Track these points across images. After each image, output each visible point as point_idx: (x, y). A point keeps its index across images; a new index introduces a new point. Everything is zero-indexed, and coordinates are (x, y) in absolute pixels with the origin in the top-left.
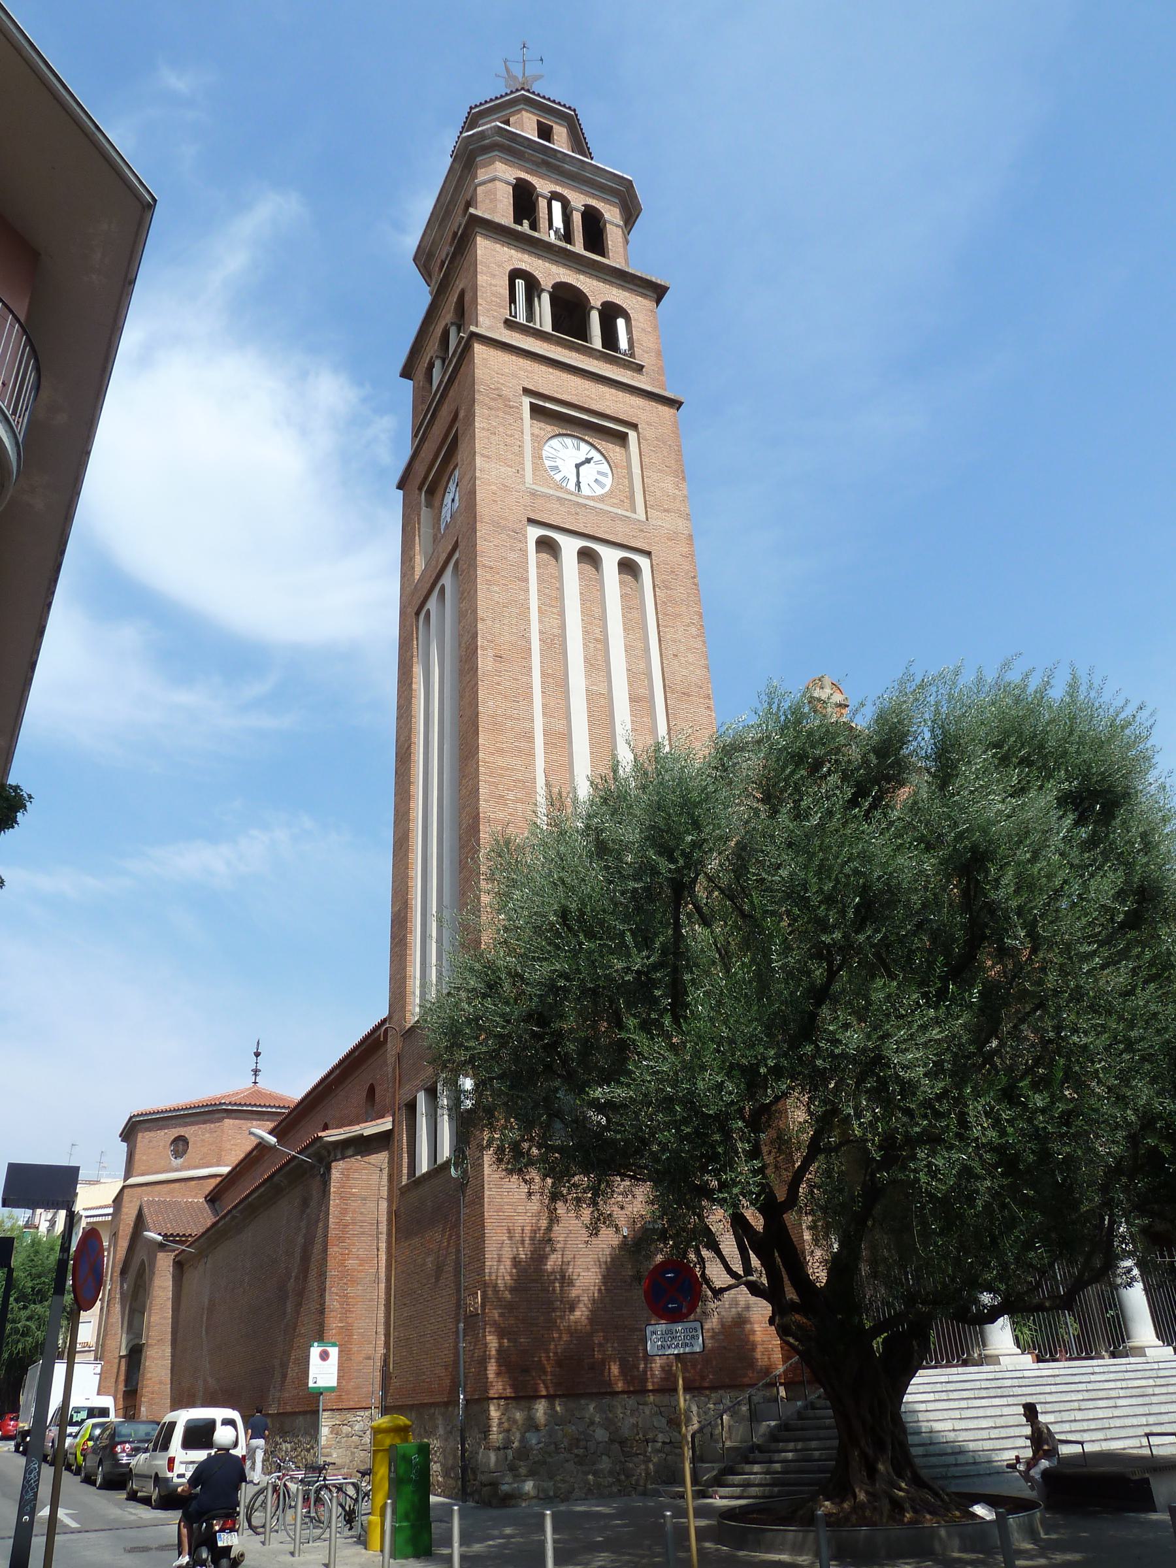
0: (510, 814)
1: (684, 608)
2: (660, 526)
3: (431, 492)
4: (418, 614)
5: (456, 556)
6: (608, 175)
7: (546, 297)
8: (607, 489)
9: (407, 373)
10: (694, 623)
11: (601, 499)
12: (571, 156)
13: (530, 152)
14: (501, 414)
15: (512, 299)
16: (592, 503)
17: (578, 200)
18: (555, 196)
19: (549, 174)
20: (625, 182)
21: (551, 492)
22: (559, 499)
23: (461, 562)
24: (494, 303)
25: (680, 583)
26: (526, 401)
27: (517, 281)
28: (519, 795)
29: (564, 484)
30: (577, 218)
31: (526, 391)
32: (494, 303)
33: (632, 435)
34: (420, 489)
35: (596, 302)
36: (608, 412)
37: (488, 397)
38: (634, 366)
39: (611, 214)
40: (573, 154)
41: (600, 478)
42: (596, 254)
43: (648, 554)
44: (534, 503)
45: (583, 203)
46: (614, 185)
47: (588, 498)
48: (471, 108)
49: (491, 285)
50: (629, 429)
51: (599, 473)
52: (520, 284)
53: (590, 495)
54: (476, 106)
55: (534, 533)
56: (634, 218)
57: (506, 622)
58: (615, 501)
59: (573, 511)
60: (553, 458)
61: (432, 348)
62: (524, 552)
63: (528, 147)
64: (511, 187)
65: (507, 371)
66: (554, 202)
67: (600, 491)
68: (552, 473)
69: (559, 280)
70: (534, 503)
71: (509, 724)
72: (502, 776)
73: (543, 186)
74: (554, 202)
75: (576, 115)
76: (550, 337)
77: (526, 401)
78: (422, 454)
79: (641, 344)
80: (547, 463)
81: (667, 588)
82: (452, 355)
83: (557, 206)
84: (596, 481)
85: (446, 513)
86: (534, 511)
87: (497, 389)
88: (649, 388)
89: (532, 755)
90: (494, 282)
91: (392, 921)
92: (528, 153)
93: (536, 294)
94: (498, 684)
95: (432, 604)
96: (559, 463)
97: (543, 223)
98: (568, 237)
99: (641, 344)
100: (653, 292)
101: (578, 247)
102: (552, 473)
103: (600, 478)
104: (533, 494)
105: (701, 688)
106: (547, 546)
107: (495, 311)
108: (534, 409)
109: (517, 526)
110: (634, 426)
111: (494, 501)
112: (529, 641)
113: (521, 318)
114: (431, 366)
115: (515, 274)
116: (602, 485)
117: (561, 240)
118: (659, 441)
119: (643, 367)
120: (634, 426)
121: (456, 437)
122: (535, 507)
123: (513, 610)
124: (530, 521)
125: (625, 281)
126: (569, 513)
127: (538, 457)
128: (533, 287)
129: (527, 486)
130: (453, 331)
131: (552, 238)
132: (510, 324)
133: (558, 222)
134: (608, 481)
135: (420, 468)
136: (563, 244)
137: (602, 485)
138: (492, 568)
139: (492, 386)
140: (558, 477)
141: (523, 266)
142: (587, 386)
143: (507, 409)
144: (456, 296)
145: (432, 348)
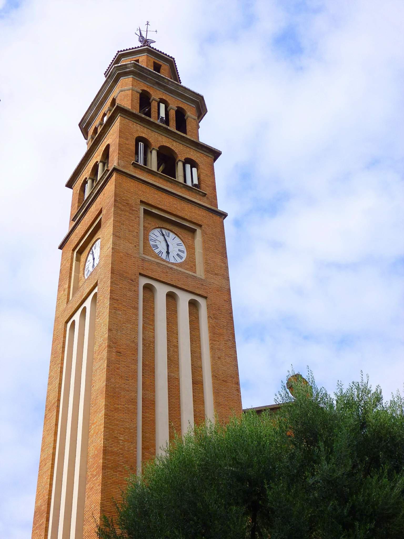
0: (121, 449)
1: (225, 331)
2: (213, 283)
3: (80, 252)
4: (67, 322)
5: (96, 290)
6: (191, 93)
7: (154, 153)
8: (183, 260)
9: (70, 185)
10: (230, 340)
11: (180, 265)
12: (153, 72)
13: (150, 77)
14: (127, 214)
15: (137, 153)
16: (175, 267)
17: (174, 103)
18: (162, 101)
19: (159, 89)
20: (200, 97)
21: (153, 259)
22: (158, 263)
23: (98, 296)
24: (127, 154)
25: (223, 316)
26: (142, 208)
27: (140, 143)
28: (126, 438)
29: (160, 255)
30: (172, 114)
31: (142, 202)
32: (127, 154)
33: (199, 232)
34: (74, 250)
35: (181, 157)
36: (186, 217)
37: (121, 204)
38: (201, 193)
39: (190, 113)
40: (154, 72)
41: (180, 253)
42: (182, 133)
43: (206, 298)
44: (143, 265)
45: (142, 89)
46: (194, 98)
47: (173, 264)
48: (118, 52)
49: (126, 144)
50: (197, 228)
51: (179, 250)
52: (141, 145)
53: (174, 262)
54: (121, 51)
55: (143, 281)
56: (203, 116)
57: (124, 332)
58: (188, 267)
59: (165, 271)
60: (155, 241)
61: (86, 173)
62: (137, 292)
63: (150, 75)
64: (157, 103)
65: (132, 190)
66: (161, 104)
67: (179, 260)
68: (154, 249)
69: (162, 144)
70: (143, 265)
71: (123, 393)
72: (117, 425)
73: (156, 94)
74: (161, 104)
75: (175, 61)
76: (156, 174)
77: (142, 208)
78: (76, 231)
79: (205, 182)
80: (151, 243)
81: (216, 318)
82: (101, 179)
83: (162, 106)
84: (178, 255)
85: (89, 266)
86: (143, 269)
87: (126, 200)
88: (209, 206)
89: (136, 413)
90: (127, 142)
91: (35, 512)
92: (149, 78)
93: (149, 151)
94: (118, 369)
95: (77, 317)
96: (157, 243)
97: (154, 114)
98: (167, 121)
99: (205, 182)
100: (212, 155)
101: (172, 127)
102: (154, 249)
103: (180, 253)
104: (143, 260)
105: (233, 378)
106: (148, 289)
107: (127, 158)
108: (146, 211)
109: (133, 277)
110: (200, 226)
111: (121, 262)
112: (137, 345)
113: (141, 162)
114: (85, 182)
115: (139, 139)
116: (181, 258)
117: (164, 124)
118: (213, 236)
119: (206, 194)
120: (200, 226)
121: (99, 224)
122: (144, 267)
123: (129, 325)
124: (141, 274)
125: (198, 148)
126: (163, 272)
127: (146, 239)
128: (147, 145)
129: (141, 255)
130: (100, 166)
131: (158, 122)
132: (135, 165)
133: (163, 114)
134: (184, 255)
135: (75, 239)
136: (164, 125)
137: (181, 258)
138: (118, 300)
139: (124, 198)
140: (157, 251)
141: (144, 135)
142: (175, 203)
143: (131, 211)
144: (104, 147)
145: (86, 173)
